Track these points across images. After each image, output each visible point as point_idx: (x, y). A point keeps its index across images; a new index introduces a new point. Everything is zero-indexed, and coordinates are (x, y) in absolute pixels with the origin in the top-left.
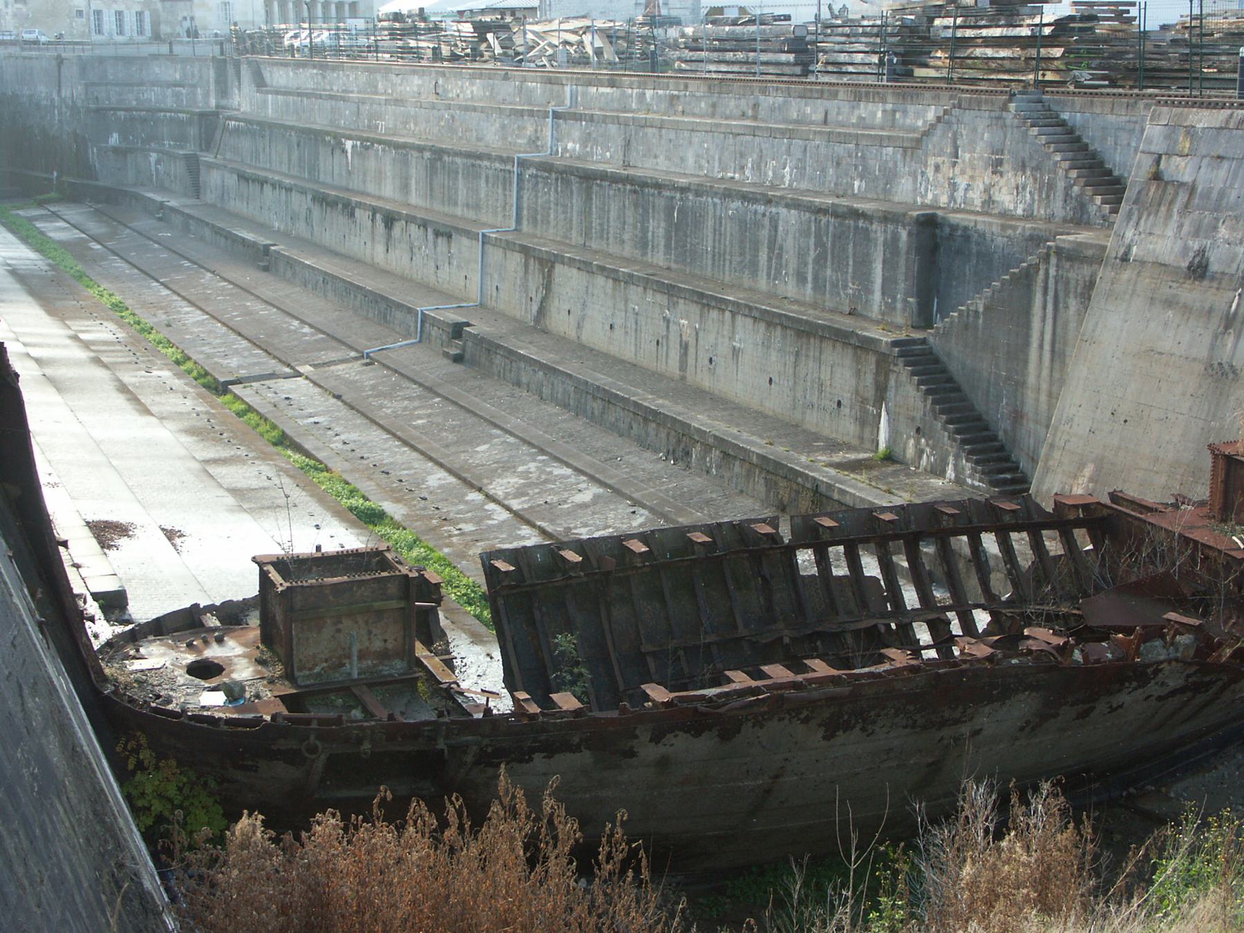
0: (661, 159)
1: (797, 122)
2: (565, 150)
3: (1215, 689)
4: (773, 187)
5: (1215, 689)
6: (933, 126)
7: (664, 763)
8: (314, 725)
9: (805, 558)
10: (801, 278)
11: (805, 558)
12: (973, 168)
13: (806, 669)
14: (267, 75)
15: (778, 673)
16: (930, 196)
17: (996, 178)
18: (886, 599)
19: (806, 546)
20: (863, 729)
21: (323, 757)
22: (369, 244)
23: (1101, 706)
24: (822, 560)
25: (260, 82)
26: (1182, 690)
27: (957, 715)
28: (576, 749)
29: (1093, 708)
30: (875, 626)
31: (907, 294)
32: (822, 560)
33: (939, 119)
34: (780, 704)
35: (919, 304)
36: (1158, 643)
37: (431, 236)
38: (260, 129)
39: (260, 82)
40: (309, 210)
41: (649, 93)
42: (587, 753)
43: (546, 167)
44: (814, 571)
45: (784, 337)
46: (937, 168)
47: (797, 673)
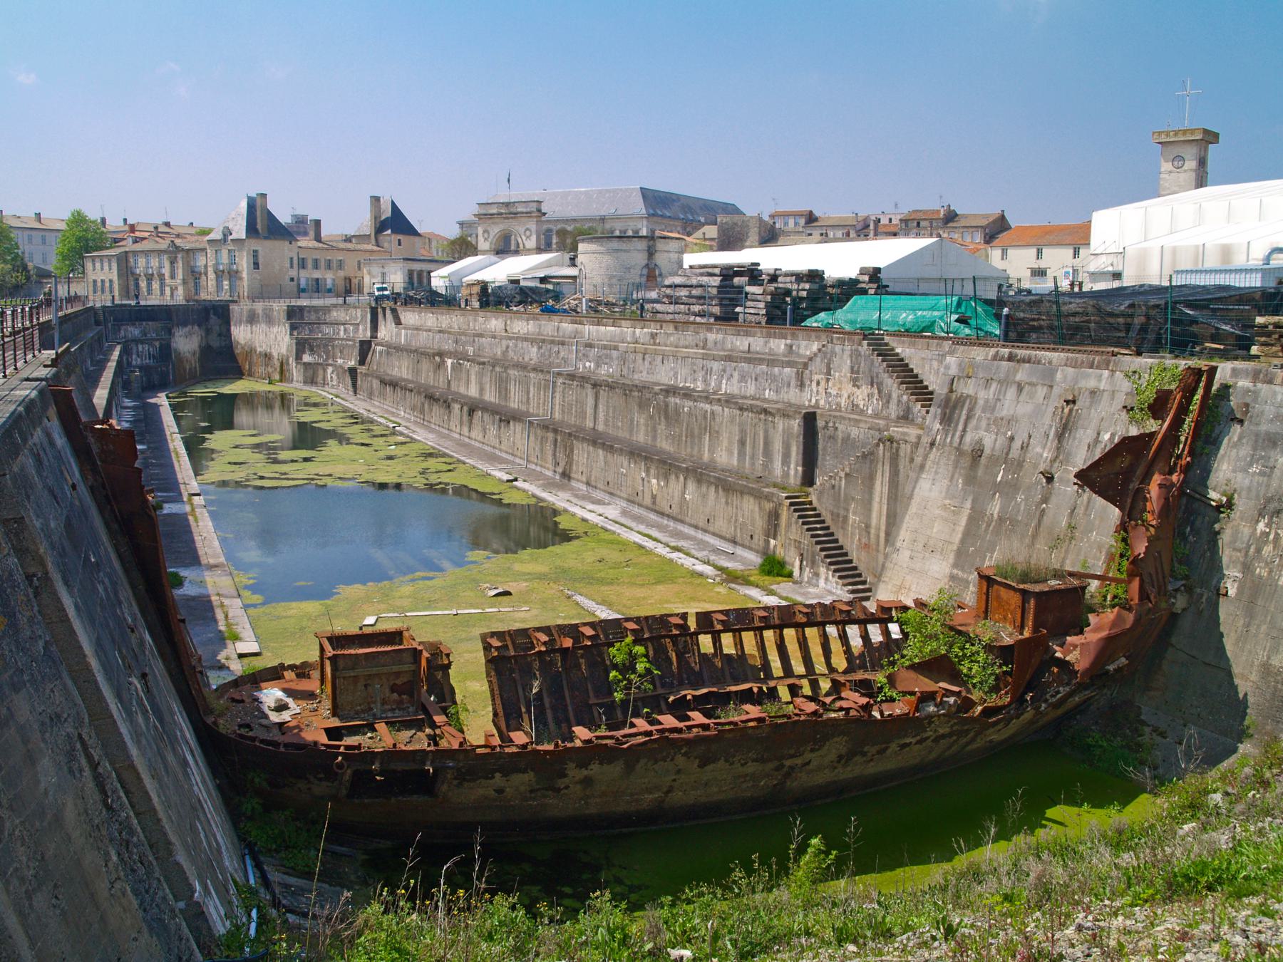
0: (644, 374)
1: (731, 350)
2: (585, 367)
3: (972, 734)
4: (715, 393)
5: (972, 734)
6: (815, 355)
7: (587, 782)
8: (342, 749)
9: (706, 642)
10: (730, 452)
11: (706, 642)
12: (841, 382)
13: (689, 718)
14: (402, 317)
15: (668, 721)
16: (814, 401)
17: (855, 389)
18: (760, 670)
19: (705, 633)
20: (726, 761)
21: (349, 771)
22: (823, 383)
23: (894, 747)
24: (717, 642)
25: (398, 322)
26: (950, 735)
27: (792, 752)
28: (525, 771)
29: (887, 748)
30: (751, 689)
31: (797, 465)
32: (717, 642)
33: (820, 350)
34: (665, 745)
35: (1133, 437)
36: (932, 703)
37: (497, 422)
38: (394, 349)
39: (398, 322)
40: (423, 405)
41: (638, 331)
42: (532, 774)
43: (572, 377)
44: (880, 639)
45: (717, 491)
46: (818, 383)
47: (680, 721)
